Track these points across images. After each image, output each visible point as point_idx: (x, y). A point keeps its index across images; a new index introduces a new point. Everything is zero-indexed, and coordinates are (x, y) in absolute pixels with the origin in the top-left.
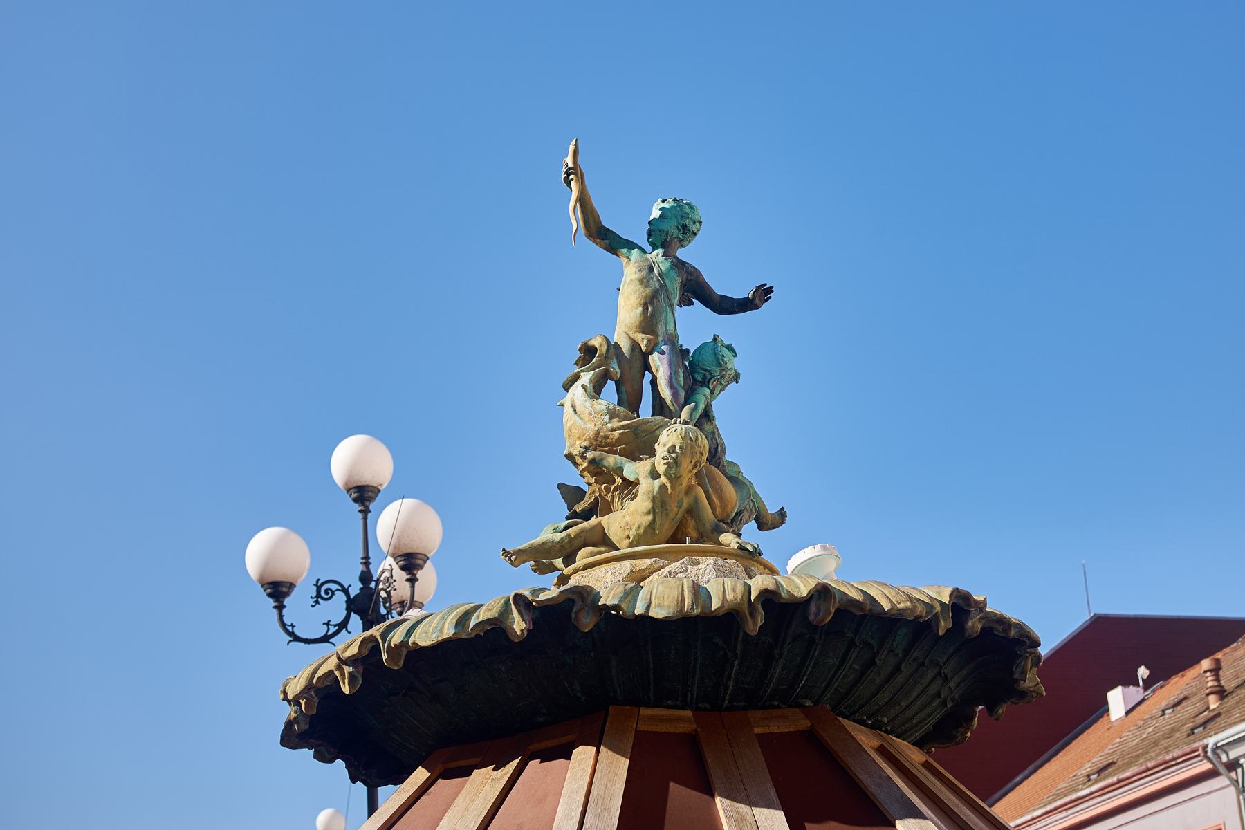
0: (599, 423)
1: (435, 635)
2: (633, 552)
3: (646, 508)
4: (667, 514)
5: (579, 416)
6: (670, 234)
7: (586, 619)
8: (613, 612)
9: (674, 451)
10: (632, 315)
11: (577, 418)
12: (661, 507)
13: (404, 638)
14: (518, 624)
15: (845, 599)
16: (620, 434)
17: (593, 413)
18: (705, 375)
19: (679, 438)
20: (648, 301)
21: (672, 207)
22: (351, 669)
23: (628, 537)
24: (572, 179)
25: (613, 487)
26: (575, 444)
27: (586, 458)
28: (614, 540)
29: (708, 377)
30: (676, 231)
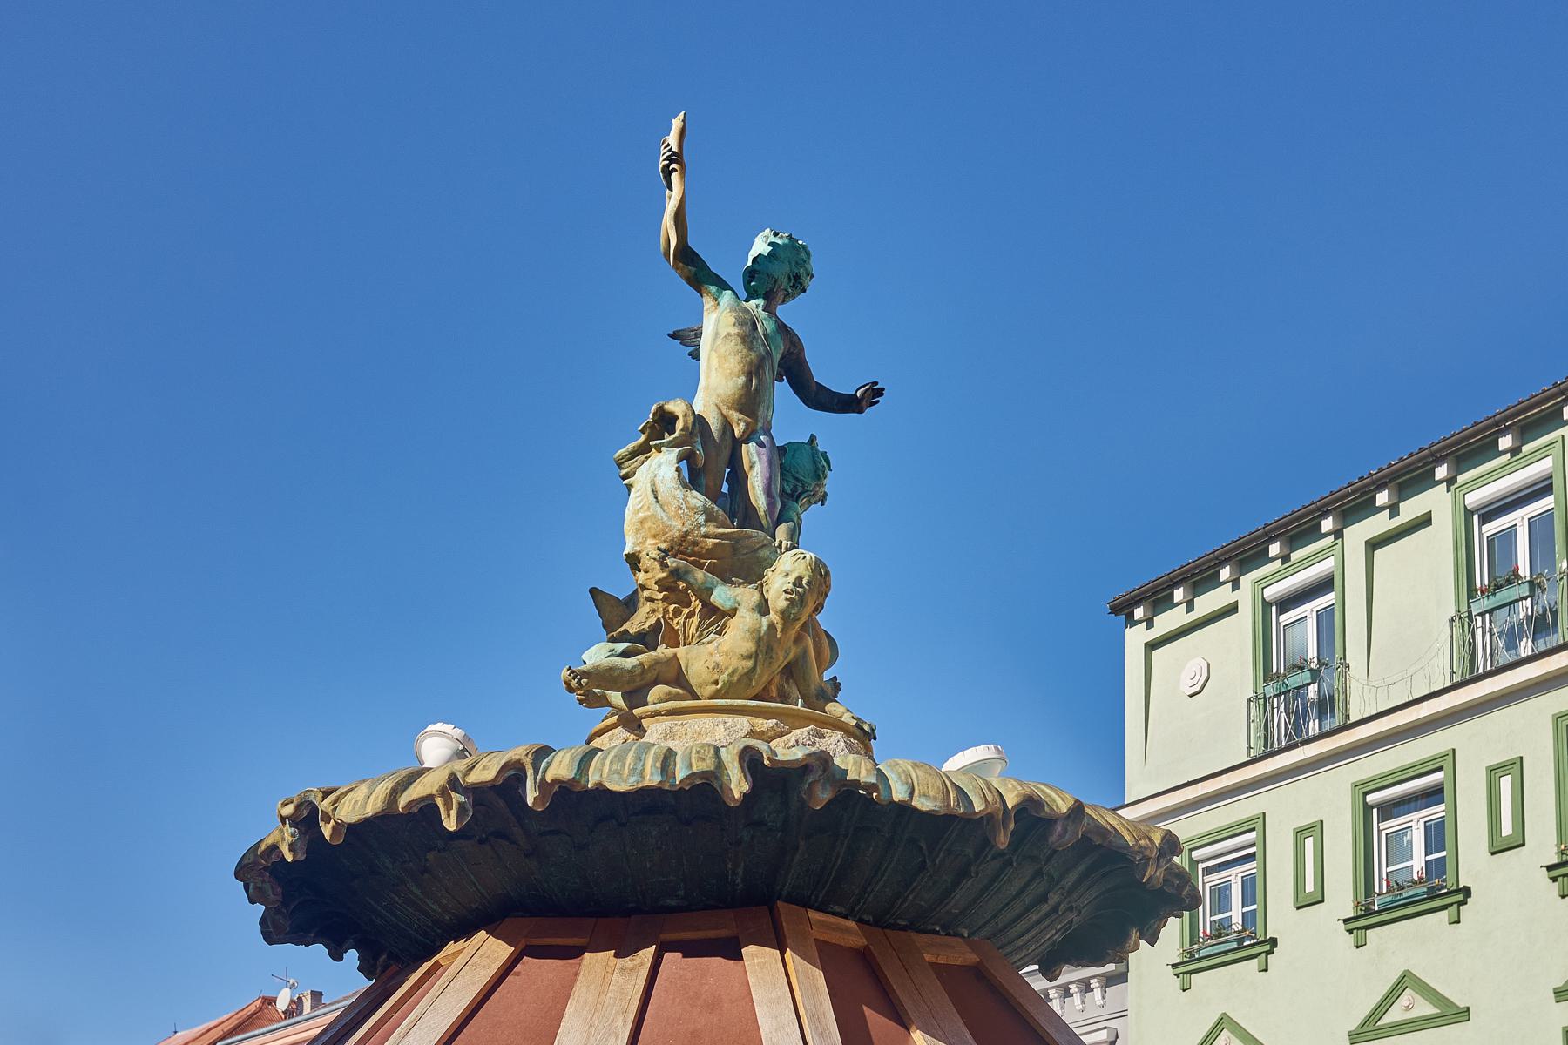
0: (689, 522)
1: (633, 779)
2: (744, 706)
3: (747, 650)
4: (770, 663)
5: (661, 506)
6: (779, 282)
7: (823, 793)
8: (861, 792)
9: (801, 586)
10: (731, 384)
11: (659, 510)
12: (766, 653)
13: (576, 775)
14: (738, 784)
15: (1092, 824)
16: (716, 544)
17: (684, 507)
18: (795, 486)
19: (807, 569)
20: (753, 369)
21: (785, 245)
22: (463, 799)
23: (716, 683)
24: (674, 170)
25: (686, 611)
26: (644, 542)
27: (667, 566)
28: (693, 682)
29: (800, 489)
30: (785, 281)
